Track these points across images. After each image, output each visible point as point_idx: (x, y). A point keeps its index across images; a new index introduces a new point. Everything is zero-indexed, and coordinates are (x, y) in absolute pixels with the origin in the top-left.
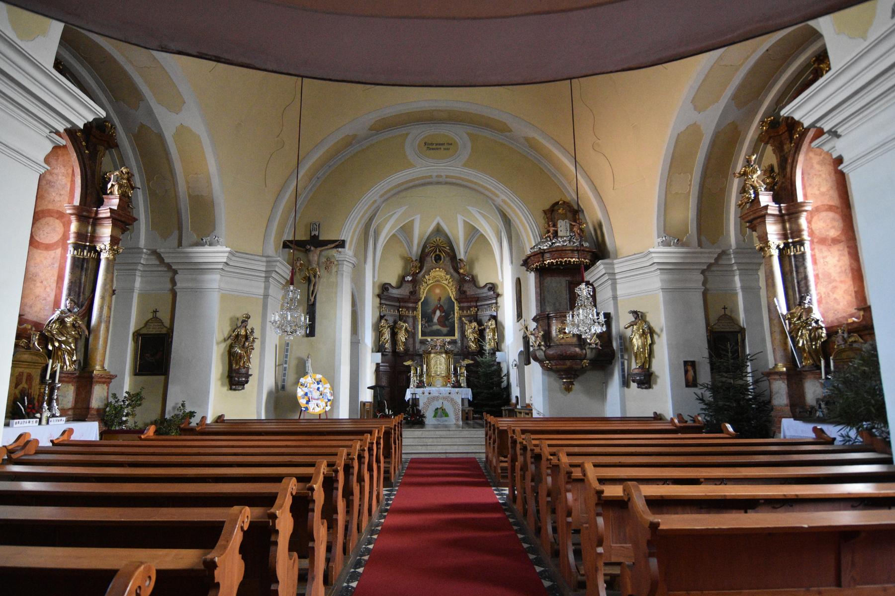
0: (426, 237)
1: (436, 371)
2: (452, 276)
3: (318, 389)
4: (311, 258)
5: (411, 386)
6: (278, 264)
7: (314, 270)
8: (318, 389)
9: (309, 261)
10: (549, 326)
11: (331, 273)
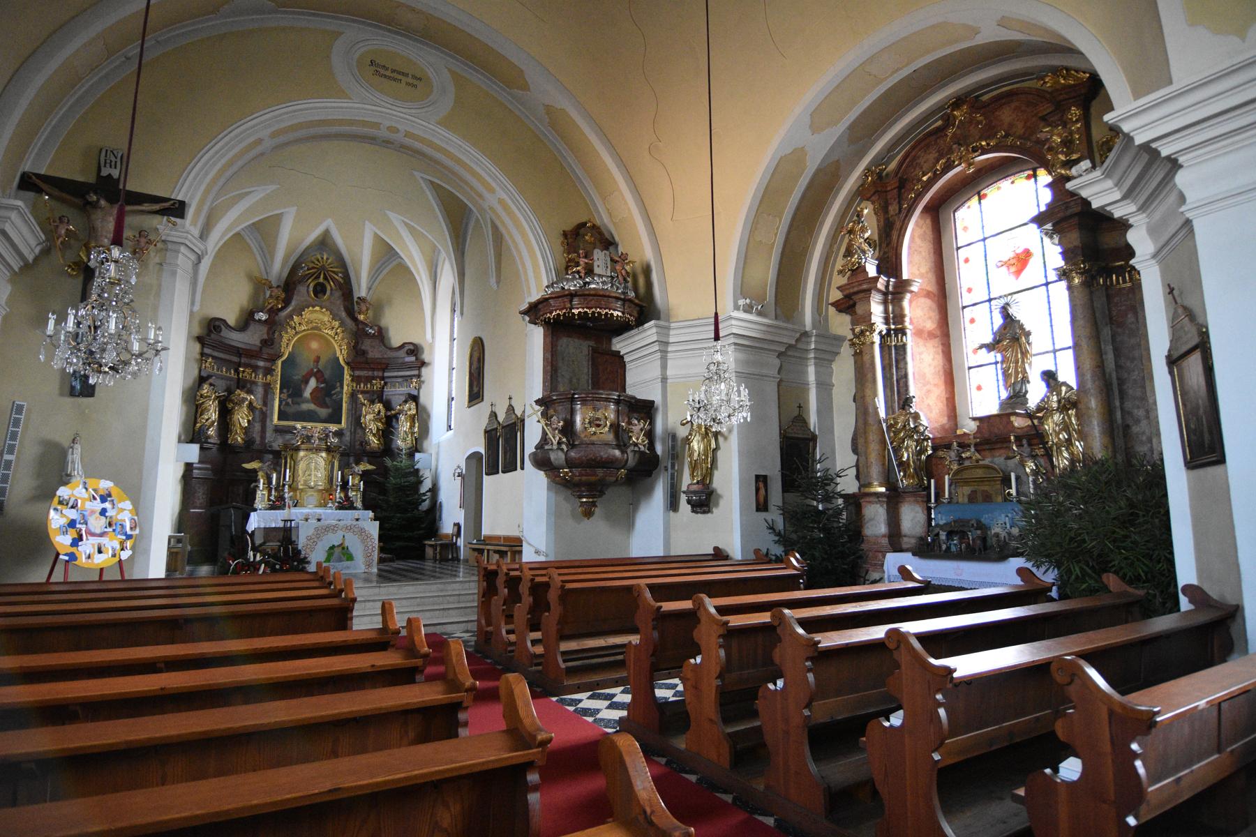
1: (306, 483)
2: (342, 324)
4: (98, 224)
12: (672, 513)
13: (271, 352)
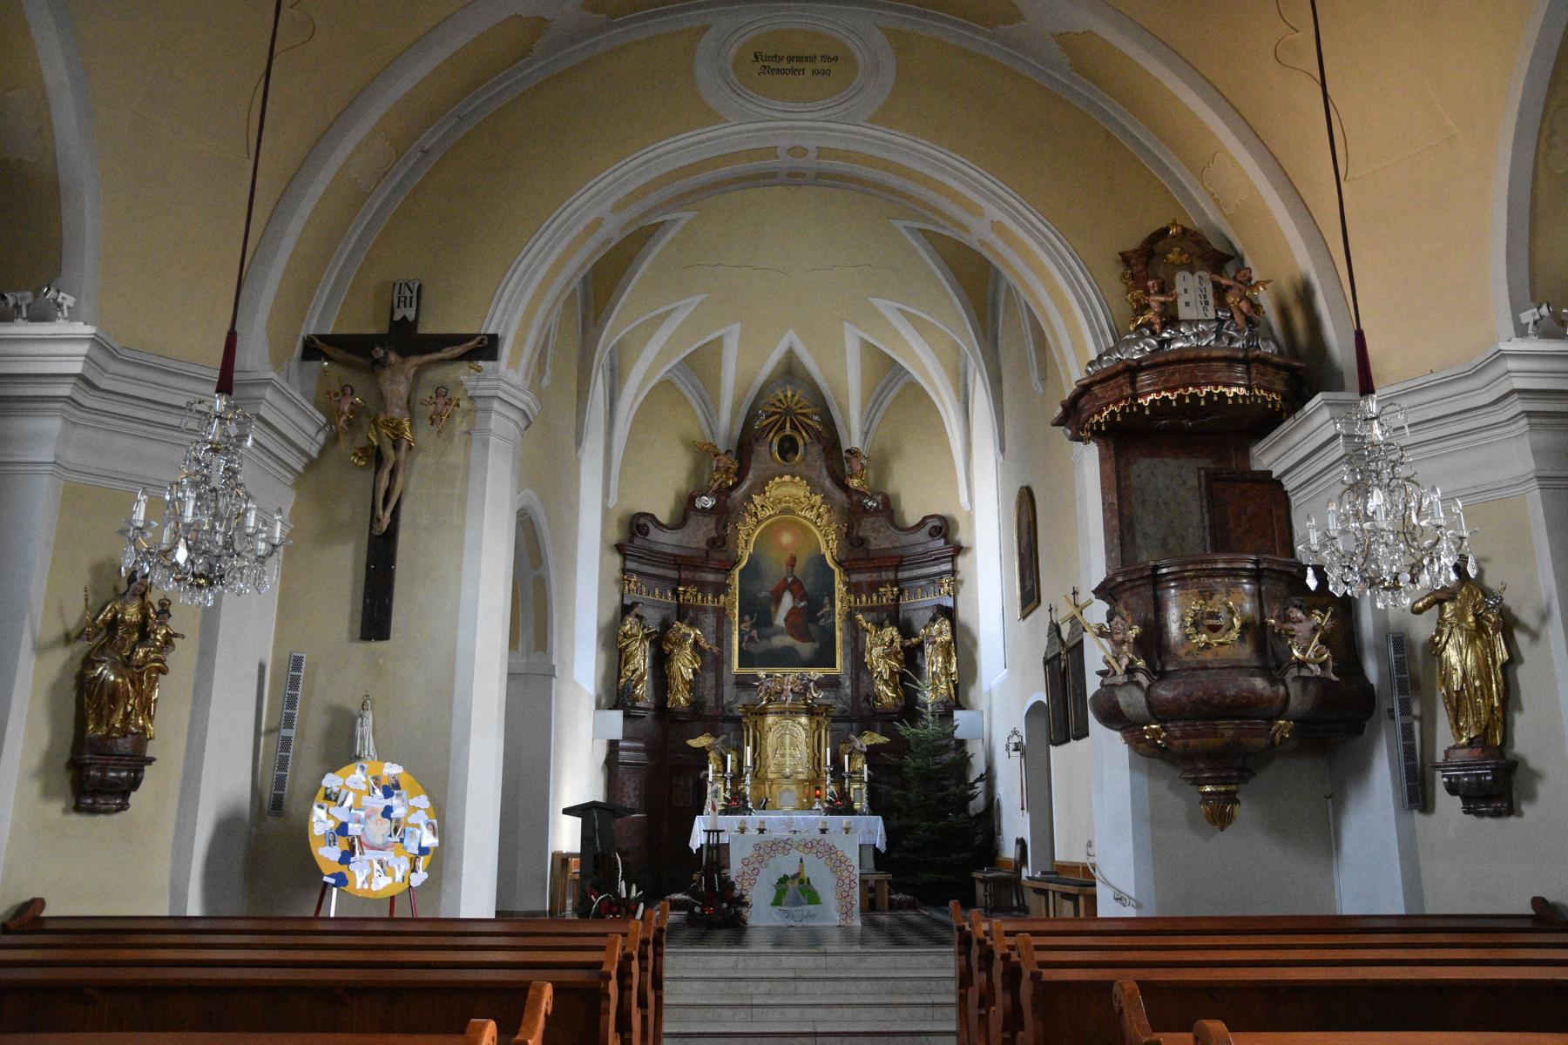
0: (753, 391)
1: (780, 766)
2: (827, 499)
3: (387, 812)
4: (387, 387)
5: (708, 808)
6: (268, 393)
7: (396, 428)
8: (387, 812)
9: (381, 398)
10: (1159, 607)
11: (450, 438)
12: (1418, 817)
13: (723, 556)
